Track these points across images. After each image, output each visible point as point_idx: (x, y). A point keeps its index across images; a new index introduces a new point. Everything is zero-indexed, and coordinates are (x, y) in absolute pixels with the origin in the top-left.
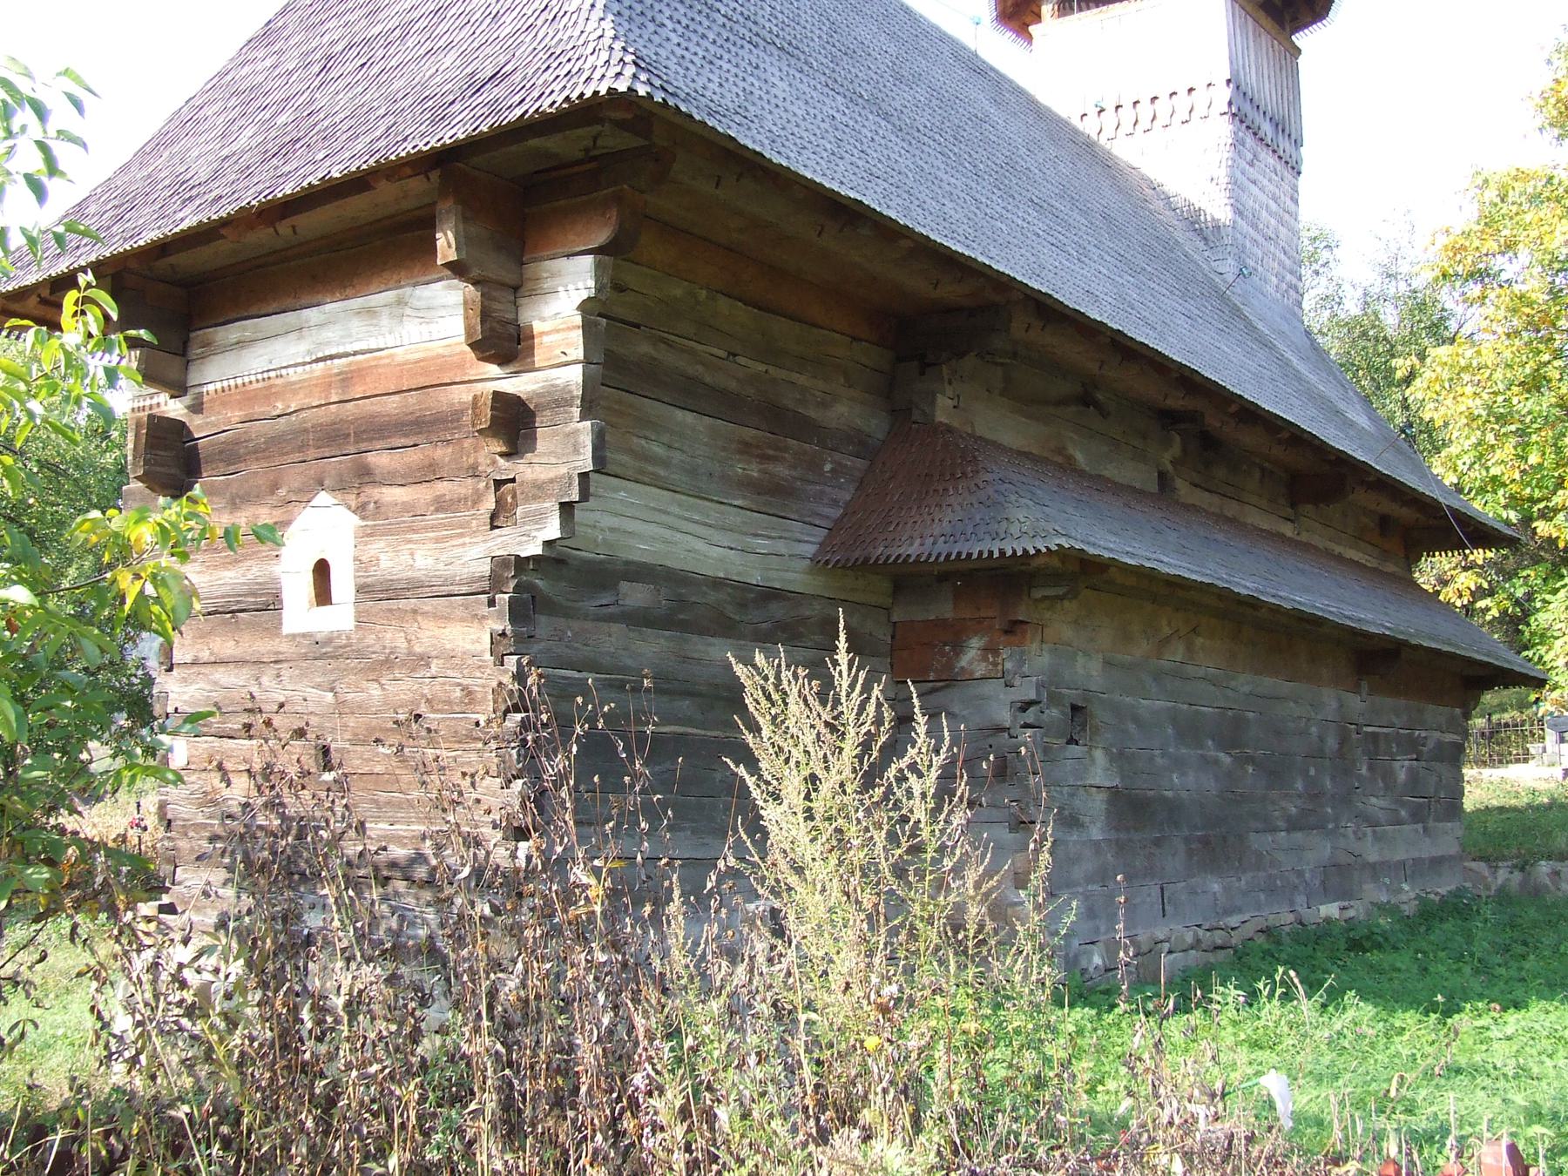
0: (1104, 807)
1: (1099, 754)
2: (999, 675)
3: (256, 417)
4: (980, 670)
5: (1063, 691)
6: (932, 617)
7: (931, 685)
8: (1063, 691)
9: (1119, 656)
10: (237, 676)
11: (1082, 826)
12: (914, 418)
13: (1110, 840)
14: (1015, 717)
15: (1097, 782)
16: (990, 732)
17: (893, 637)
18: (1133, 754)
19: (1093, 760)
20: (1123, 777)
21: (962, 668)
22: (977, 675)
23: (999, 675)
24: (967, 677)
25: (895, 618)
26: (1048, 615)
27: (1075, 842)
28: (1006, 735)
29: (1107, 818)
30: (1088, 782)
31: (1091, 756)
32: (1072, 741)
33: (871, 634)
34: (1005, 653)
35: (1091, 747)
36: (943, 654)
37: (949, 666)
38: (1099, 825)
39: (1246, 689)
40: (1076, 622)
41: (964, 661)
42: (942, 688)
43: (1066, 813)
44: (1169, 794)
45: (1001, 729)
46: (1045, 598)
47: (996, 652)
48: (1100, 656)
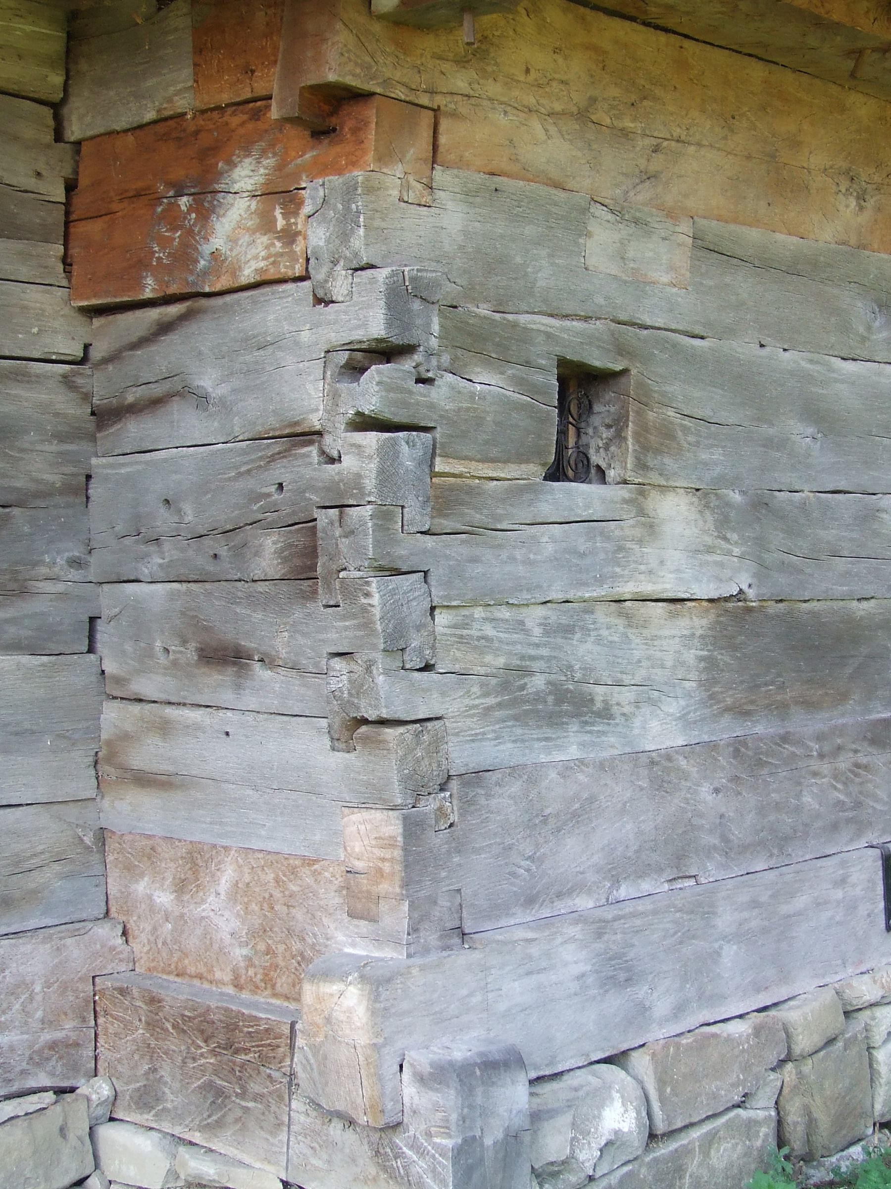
0: (691, 656)
2: (298, 270)
3: (720, 249)
5: (523, 319)
7: (154, 314)
8: (523, 319)
9: (754, 235)
10: (441, 524)
11: (606, 714)
13: (712, 747)
14: (335, 395)
15: (669, 586)
16: (277, 446)
17: (71, 187)
18: (803, 506)
19: (651, 529)
20: (763, 570)
22: (247, 275)
27: (567, 770)
29: (706, 684)
30: (627, 589)
31: (641, 512)
35: (642, 489)
40: (583, 115)
42: (165, 328)
48: (685, 227)
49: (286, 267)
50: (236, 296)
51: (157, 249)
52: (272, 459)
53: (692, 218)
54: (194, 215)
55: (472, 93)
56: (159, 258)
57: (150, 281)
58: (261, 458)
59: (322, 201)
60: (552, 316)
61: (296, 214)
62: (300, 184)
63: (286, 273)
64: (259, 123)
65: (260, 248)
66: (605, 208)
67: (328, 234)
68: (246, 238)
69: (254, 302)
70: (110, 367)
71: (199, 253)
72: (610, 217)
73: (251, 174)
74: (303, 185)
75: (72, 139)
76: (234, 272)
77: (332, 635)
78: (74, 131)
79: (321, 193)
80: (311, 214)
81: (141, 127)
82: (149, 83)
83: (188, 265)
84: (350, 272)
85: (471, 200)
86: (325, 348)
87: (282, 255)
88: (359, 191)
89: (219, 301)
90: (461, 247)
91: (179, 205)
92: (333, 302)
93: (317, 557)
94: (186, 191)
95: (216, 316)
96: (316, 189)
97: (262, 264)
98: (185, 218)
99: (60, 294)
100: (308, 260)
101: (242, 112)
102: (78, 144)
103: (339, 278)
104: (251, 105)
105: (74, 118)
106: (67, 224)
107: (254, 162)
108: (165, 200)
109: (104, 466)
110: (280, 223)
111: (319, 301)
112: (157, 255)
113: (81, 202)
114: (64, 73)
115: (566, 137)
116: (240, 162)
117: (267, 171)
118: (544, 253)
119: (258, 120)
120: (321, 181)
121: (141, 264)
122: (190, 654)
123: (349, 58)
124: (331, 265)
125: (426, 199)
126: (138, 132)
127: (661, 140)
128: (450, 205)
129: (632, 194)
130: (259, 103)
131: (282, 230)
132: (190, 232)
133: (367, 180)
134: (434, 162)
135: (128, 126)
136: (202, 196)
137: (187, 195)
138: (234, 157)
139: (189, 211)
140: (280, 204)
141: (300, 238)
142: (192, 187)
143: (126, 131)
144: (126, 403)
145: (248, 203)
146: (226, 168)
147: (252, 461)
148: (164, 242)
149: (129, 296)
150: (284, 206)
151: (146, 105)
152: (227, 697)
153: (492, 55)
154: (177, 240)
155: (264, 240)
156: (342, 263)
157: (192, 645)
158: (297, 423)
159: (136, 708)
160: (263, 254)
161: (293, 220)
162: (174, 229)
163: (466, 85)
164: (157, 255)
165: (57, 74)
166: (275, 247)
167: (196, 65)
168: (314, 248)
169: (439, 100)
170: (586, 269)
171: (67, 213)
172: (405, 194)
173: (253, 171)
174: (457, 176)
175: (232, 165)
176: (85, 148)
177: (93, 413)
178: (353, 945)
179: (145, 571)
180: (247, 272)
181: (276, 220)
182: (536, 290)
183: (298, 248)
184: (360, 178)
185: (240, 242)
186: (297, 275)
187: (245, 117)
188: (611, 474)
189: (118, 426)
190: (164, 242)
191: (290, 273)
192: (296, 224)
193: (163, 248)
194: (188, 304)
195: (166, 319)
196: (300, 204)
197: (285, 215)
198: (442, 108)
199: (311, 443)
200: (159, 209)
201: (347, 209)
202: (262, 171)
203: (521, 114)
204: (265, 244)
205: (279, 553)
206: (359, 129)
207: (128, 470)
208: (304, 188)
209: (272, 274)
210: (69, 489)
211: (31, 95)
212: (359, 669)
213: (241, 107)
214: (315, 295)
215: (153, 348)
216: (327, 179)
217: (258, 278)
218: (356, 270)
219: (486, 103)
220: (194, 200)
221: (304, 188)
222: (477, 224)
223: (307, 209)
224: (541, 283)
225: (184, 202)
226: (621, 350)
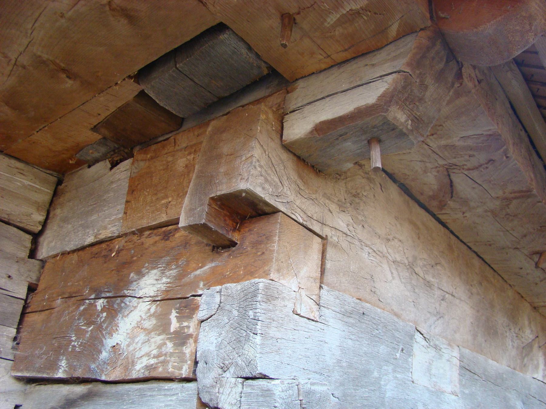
2: (185, 372)
17: (32, 289)
40: (411, 267)
49: (174, 367)
50: (127, 387)
51: (74, 339)
53: (458, 346)
54: (105, 314)
55: (348, 233)
56: (74, 346)
57: (63, 363)
59: (217, 306)
61: (189, 317)
62: (196, 291)
63: (173, 373)
64: (168, 242)
65: (153, 347)
66: (421, 336)
67: (220, 339)
68: (142, 337)
69: (142, 396)
71: (103, 345)
72: (424, 343)
73: (155, 282)
74: (200, 292)
75: (41, 258)
76: (130, 363)
78: (43, 252)
79: (217, 299)
80: (204, 318)
81: (83, 248)
82: (94, 217)
83: (93, 355)
84: (240, 380)
85: (346, 319)
87: (171, 354)
88: (259, 298)
90: (339, 361)
91: (96, 306)
94: (103, 295)
95: (108, 402)
96: (212, 296)
97: (153, 361)
98: (98, 316)
99: (4, 365)
100: (196, 363)
101: (156, 235)
102: (43, 262)
103: (228, 385)
104: (164, 229)
105: (45, 244)
106: (23, 314)
107: (159, 273)
108: (87, 301)
110: (174, 325)
112: (73, 343)
113: (36, 301)
114: (45, 214)
115: (403, 280)
116: (148, 273)
117: (168, 280)
118: (390, 368)
119: (167, 240)
120: (218, 288)
121: (59, 351)
123: (261, 172)
124: (220, 371)
125: (315, 315)
126: (81, 253)
127: (445, 293)
128: (332, 322)
129: (433, 327)
130: (170, 227)
131: (176, 332)
132: (99, 328)
133: (267, 288)
134: (321, 282)
135: (75, 248)
136: (113, 299)
137: (103, 298)
138: (143, 269)
139: (103, 310)
140: (176, 309)
141: (191, 341)
142: (108, 292)
143: (74, 251)
145: (149, 307)
146: (135, 277)
148: (80, 333)
149: (48, 373)
150: (180, 311)
151: (89, 232)
153: (362, 208)
154: (89, 333)
155: (159, 339)
156: (232, 370)
160: (155, 352)
161: (185, 324)
162: (88, 324)
163: (345, 226)
164: (73, 343)
165: (40, 214)
166: (167, 347)
168: (204, 352)
169: (326, 231)
170: (413, 382)
171: (25, 308)
172: (298, 306)
173: (157, 280)
174: (338, 298)
175: (141, 275)
176: (47, 266)
180: (138, 367)
181: (169, 324)
182: (386, 400)
183: (188, 350)
184: (261, 286)
185: (136, 340)
186: (184, 376)
187: (157, 238)
190: (80, 333)
191: (176, 374)
192: (188, 327)
193: (78, 338)
194: (89, 386)
195: (71, 396)
196: (195, 308)
197: (180, 319)
198: (329, 238)
201: (243, 315)
202: (165, 280)
203: (378, 257)
204: (157, 344)
206: (260, 243)
208: (200, 296)
209: (160, 372)
211: (18, 224)
213: (155, 231)
214: (199, 399)
216: (223, 286)
217: (147, 374)
218: (247, 378)
219: (357, 243)
220: (107, 302)
221: (200, 296)
222: (350, 341)
223: (201, 314)
224: (389, 394)
225: (100, 304)
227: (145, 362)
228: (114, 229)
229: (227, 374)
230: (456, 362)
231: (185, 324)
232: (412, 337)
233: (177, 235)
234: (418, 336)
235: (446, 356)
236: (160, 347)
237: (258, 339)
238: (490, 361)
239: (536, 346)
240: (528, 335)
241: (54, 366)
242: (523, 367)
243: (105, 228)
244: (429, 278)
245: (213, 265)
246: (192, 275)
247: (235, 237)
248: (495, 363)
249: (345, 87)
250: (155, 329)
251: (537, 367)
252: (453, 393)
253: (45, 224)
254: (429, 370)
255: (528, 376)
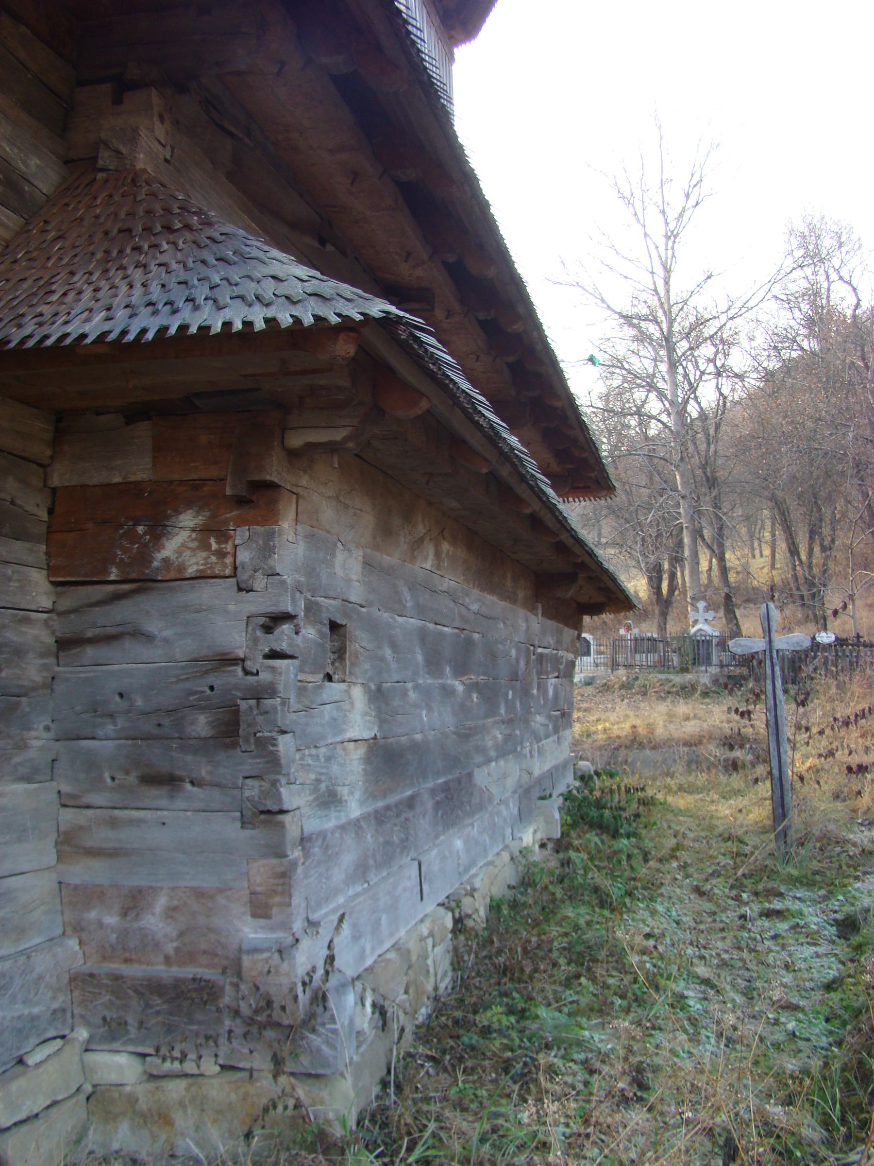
1: (357, 693)
2: (228, 572)
4: (194, 564)
6: (117, 479)
7: (111, 588)
12: (100, 163)
14: (255, 641)
15: (351, 734)
17: (51, 512)
21: (166, 560)
22: (191, 571)
23: (228, 572)
24: (172, 575)
25: (56, 481)
26: (304, 481)
28: (239, 670)
31: (350, 697)
32: (329, 678)
33: (13, 502)
34: (241, 535)
36: (134, 538)
37: (144, 557)
38: (357, 795)
39: (474, 607)
40: (337, 498)
41: (169, 549)
42: (117, 597)
43: (323, 786)
44: (418, 737)
45: (227, 661)
46: (311, 447)
47: (223, 536)
52: (206, 672)
58: (197, 672)
60: (325, 597)
70: (72, 616)
72: (342, 548)
77: (246, 767)
86: (248, 615)
87: (216, 563)
89: (159, 585)
92: (252, 591)
93: (239, 725)
105: (55, 475)
109: (65, 672)
110: (214, 546)
111: (240, 589)
118: (324, 566)
122: (132, 779)
132: (146, 545)
144: (86, 637)
147: (189, 673)
148: (125, 550)
152: (164, 803)
155: (204, 554)
157: (134, 774)
158: (225, 654)
159: (90, 812)
160: (202, 562)
167: (154, 457)
175: (178, 513)
177: (56, 641)
178: (256, 932)
179: (100, 733)
180: (190, 571)
181: (210, 545)
188: (336, 677)
189: (78, 650)
191: (222, 574)
193: (124, 553)
197: (218, 543)
199: (236, 664)
200: (121, 531)
205: (209, 723)
207: (86, 675)
210: (45, 686)
212: (266, 785)
215: (108, 608)
217: (198, 574)
224: (324, 582)
225: (140, 529)
226: (346, 615)
227: (195, 568)
228: (144, 476)
229: (257, 574)
230: (361, 559)
231: (223, 546)
232: (336, 545)
233: (205, 489)
234: (339, 544)
235: (354, 555)
236: (205, 559)
237: (276, 556)
238: (385, 556)
239: (428, 538)
240: (421, 530)
241: (105, 571)
242: (413, 559)
243: (134, 473)
244: (348, 502)
245: (239, 512)
246: (223, 517)
247: (254, 498)
248: (388, 557)
249: (323, 424)
250: (198, 548)
251: (426, 558)
252: (358, 581)
253: (52, 458)
254: (344, 565)
255: (416, 568)
